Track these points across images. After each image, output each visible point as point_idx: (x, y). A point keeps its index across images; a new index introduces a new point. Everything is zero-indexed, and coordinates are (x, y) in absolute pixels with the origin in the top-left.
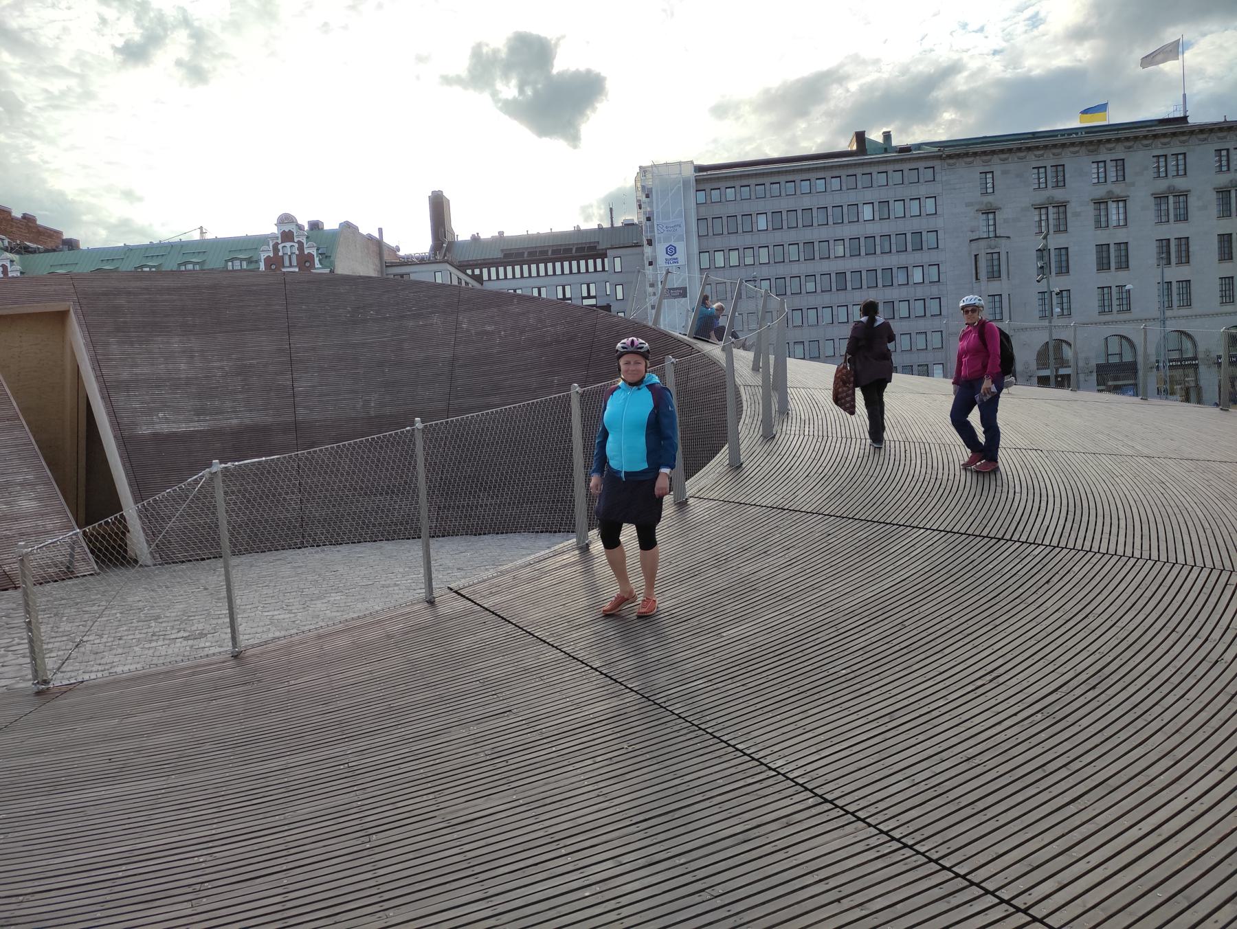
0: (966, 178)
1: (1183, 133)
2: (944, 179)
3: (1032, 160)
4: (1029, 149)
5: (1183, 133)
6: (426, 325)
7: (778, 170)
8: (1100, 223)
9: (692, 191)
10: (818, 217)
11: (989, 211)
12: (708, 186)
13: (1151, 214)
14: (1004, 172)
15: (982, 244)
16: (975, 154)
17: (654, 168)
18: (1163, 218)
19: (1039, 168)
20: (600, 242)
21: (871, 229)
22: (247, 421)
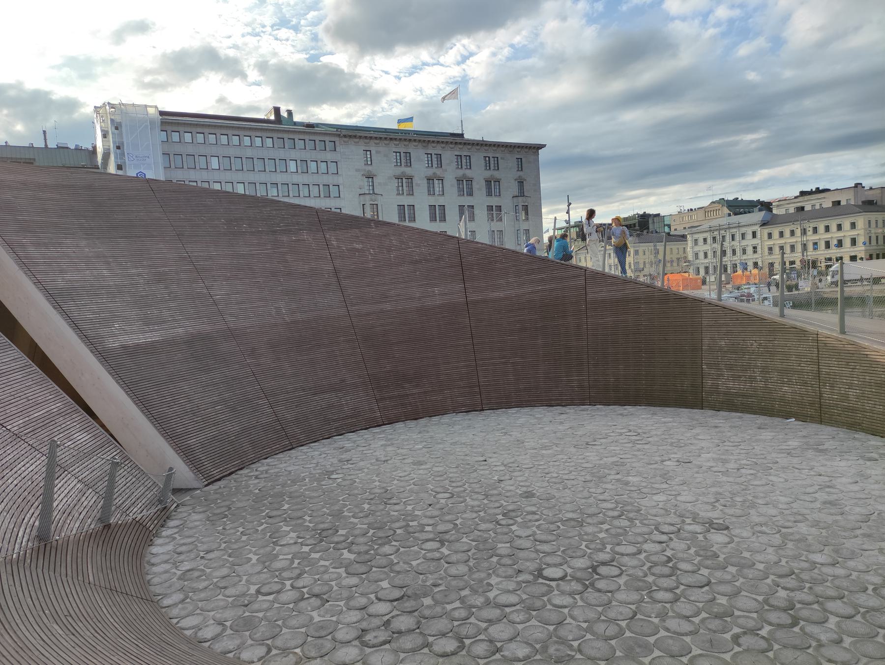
0: (353, 153)
1: (460, 143)
2: (342, 150)
3: (393, 147)
4: (391, 139)
5: (460, 143)
6: (299, 240)
7: (196, 123)
8: (431, 192)
9: (158, 130)
10: (259, 165)
11: (370, 177)
12: (169, 128)
13: (455, 190)
14: (377, 152)
15: (368, 197)
16: (360, 137)
17: (122, 107)
18: (461, 192)
19: (396, 152)
20: (36, 158)
21: (297, 179)
22: (190, 330)
